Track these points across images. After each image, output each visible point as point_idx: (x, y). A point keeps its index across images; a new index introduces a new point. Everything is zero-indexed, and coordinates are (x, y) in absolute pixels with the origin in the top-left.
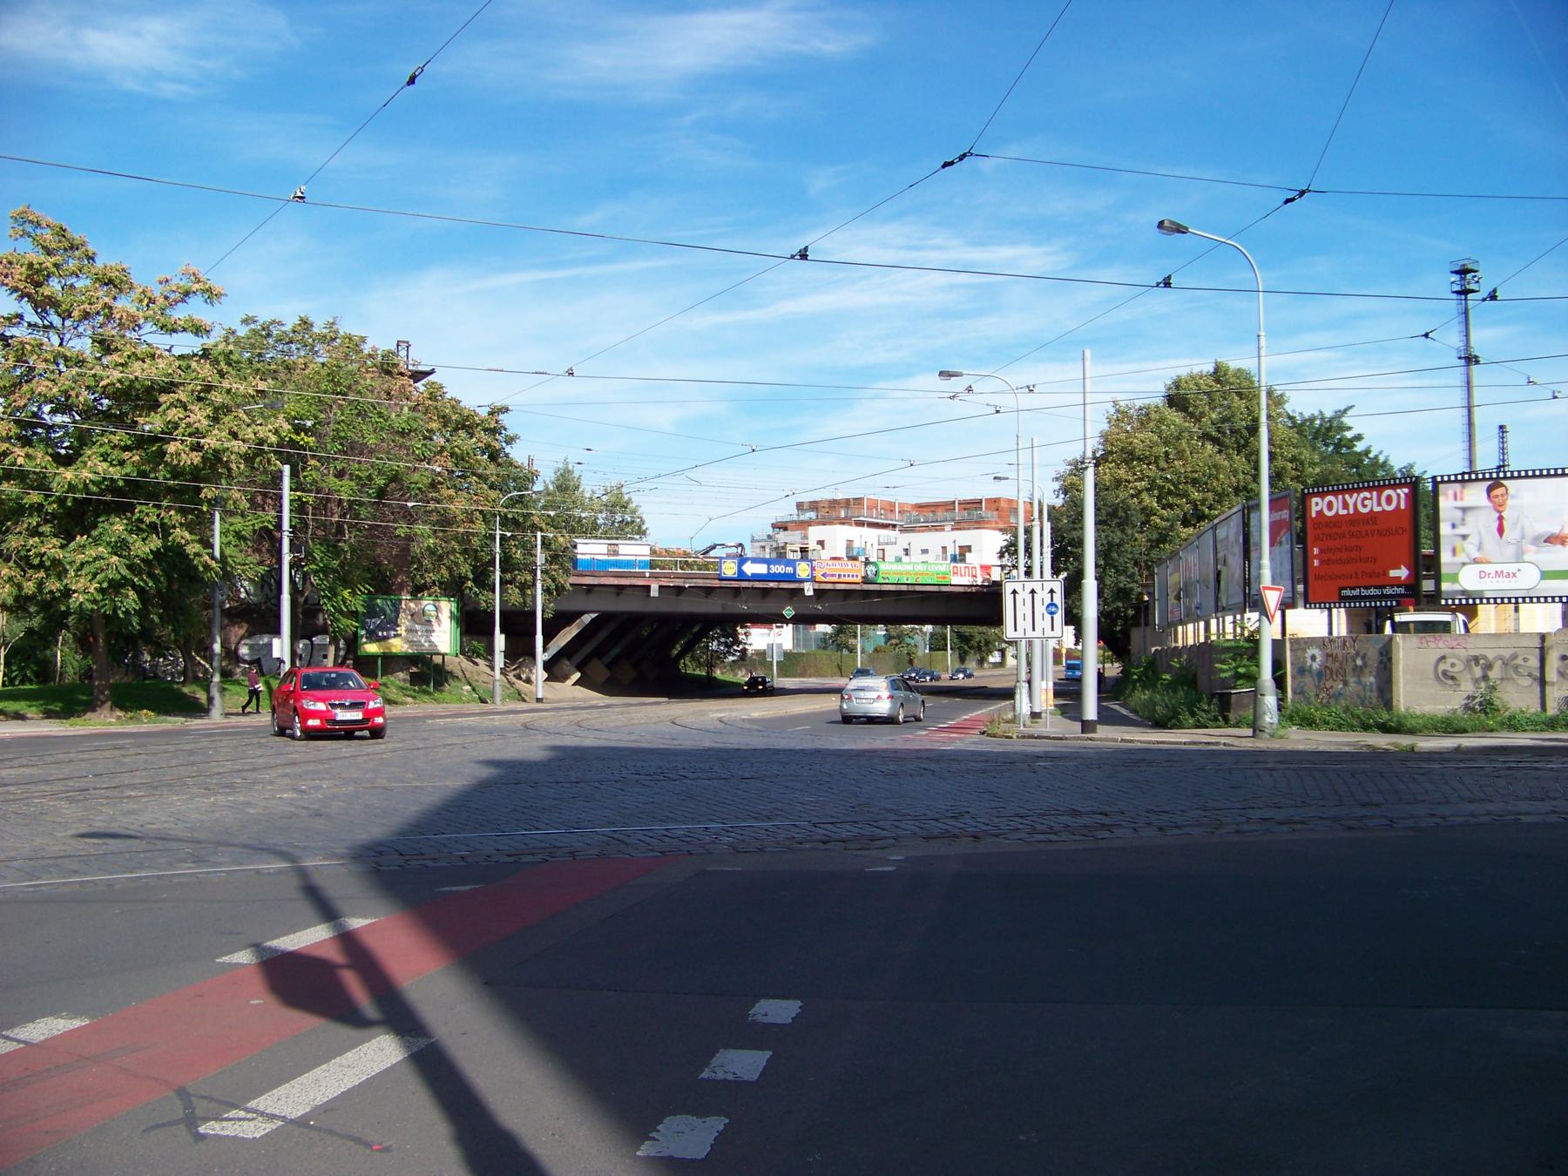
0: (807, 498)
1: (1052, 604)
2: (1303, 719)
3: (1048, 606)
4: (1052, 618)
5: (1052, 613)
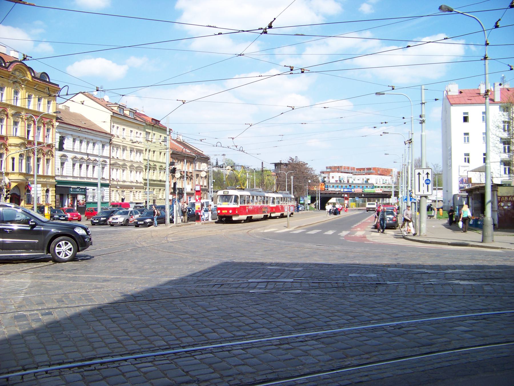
0: (328, 166)
1: (428, 180)
2: (131, 167)
3: (426, 181)
4: (428, 186)
5: (428, 184)
